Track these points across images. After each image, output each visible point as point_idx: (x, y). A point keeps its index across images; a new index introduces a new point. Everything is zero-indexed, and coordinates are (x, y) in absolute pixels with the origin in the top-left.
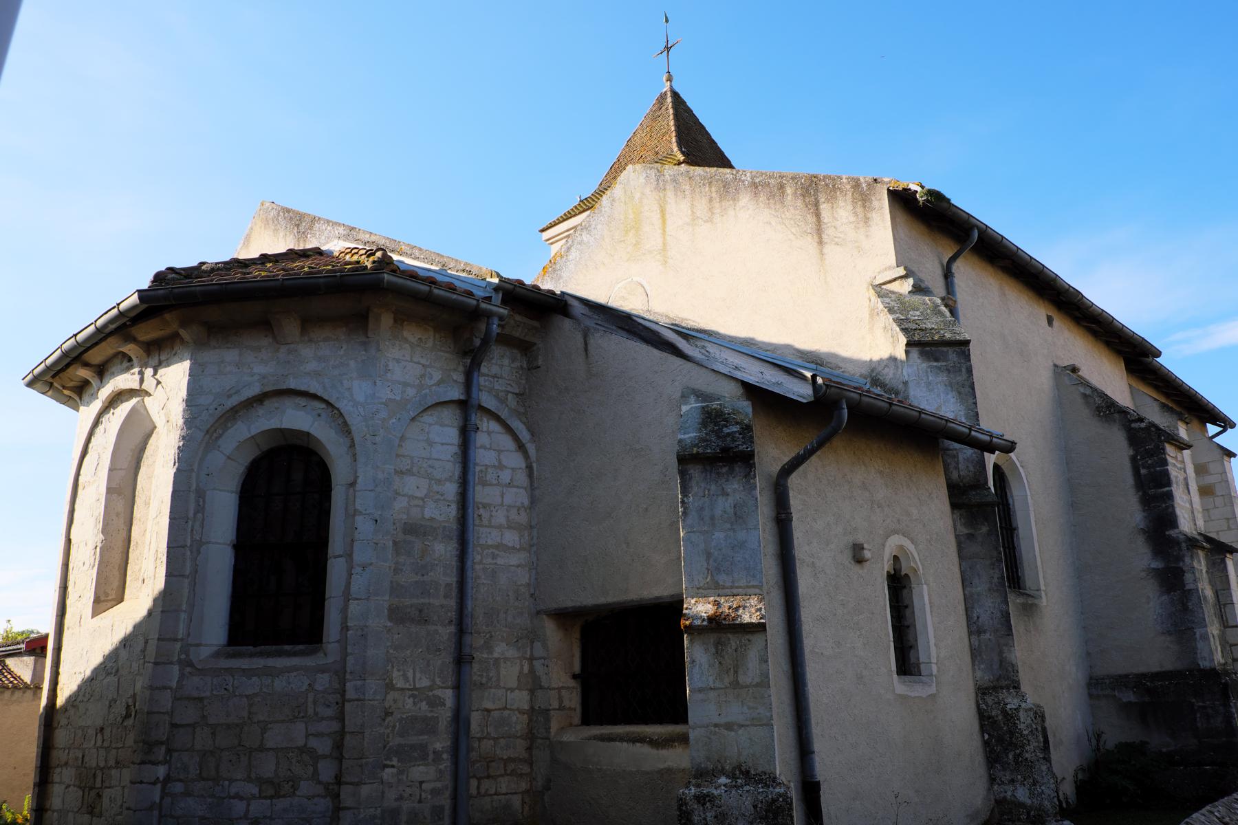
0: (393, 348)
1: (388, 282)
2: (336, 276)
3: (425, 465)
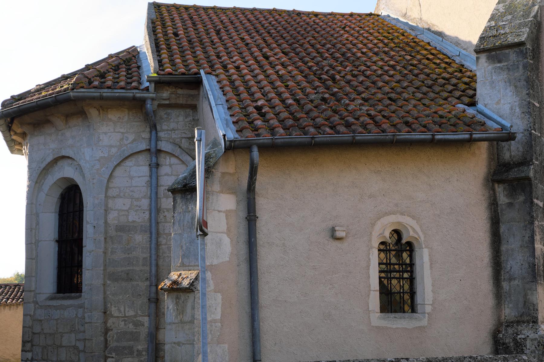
0: (102, 127)
1: (74, 97)
2: (53, 97)
3: (128, 191)
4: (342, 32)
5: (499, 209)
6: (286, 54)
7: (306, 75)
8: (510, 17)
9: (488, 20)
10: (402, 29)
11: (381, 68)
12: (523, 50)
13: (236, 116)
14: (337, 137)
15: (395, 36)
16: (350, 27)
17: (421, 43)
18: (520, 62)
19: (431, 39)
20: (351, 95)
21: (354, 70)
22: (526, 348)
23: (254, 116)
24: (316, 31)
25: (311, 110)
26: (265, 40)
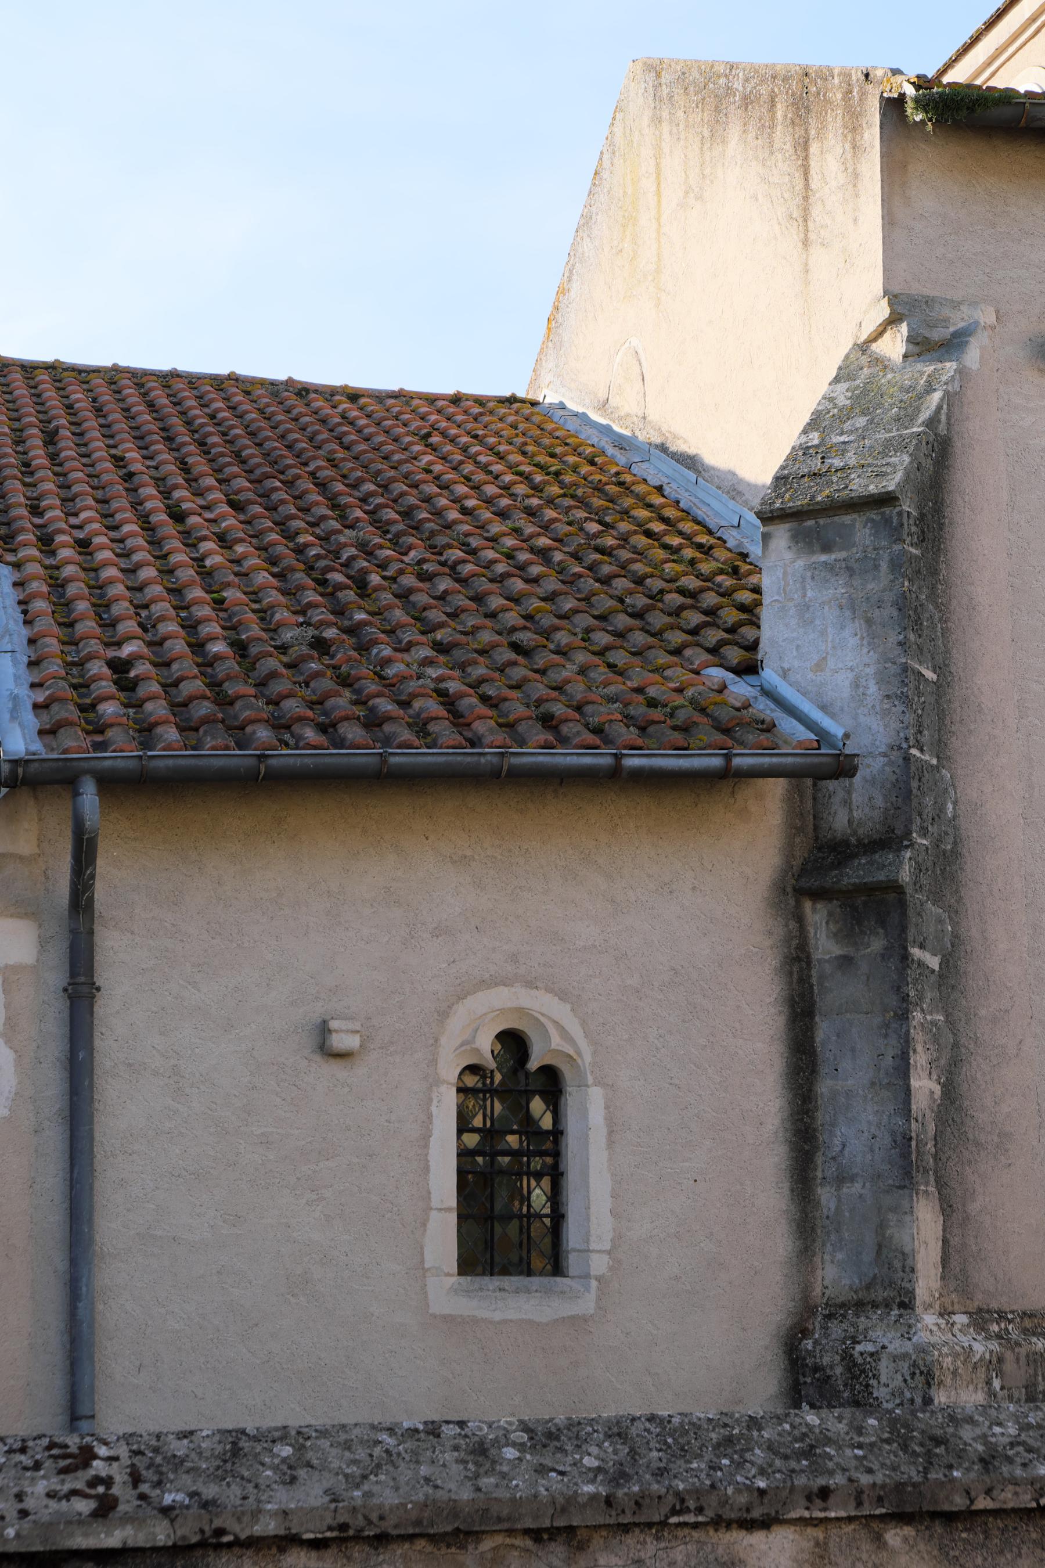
4: (417, 448)
5: (814, 973)
6: (237, 506)
7: (283, 569)
8: (861, 421)
9: (802, 428)
10: (593, 446)
11: (509, 556)
12: (891, 517)
13: (47, 689)
14: (334, 757)
15: (568, 466)
16: (443, 434)
17: (640, 488)
18: (881, 552)
19: (668, 477)
20: (404, 633)
21: (428, 561)
22: (879, 1382)
23: (99, 689)
24: (341, 443)
25: (273, 675)
26: (186, 463)
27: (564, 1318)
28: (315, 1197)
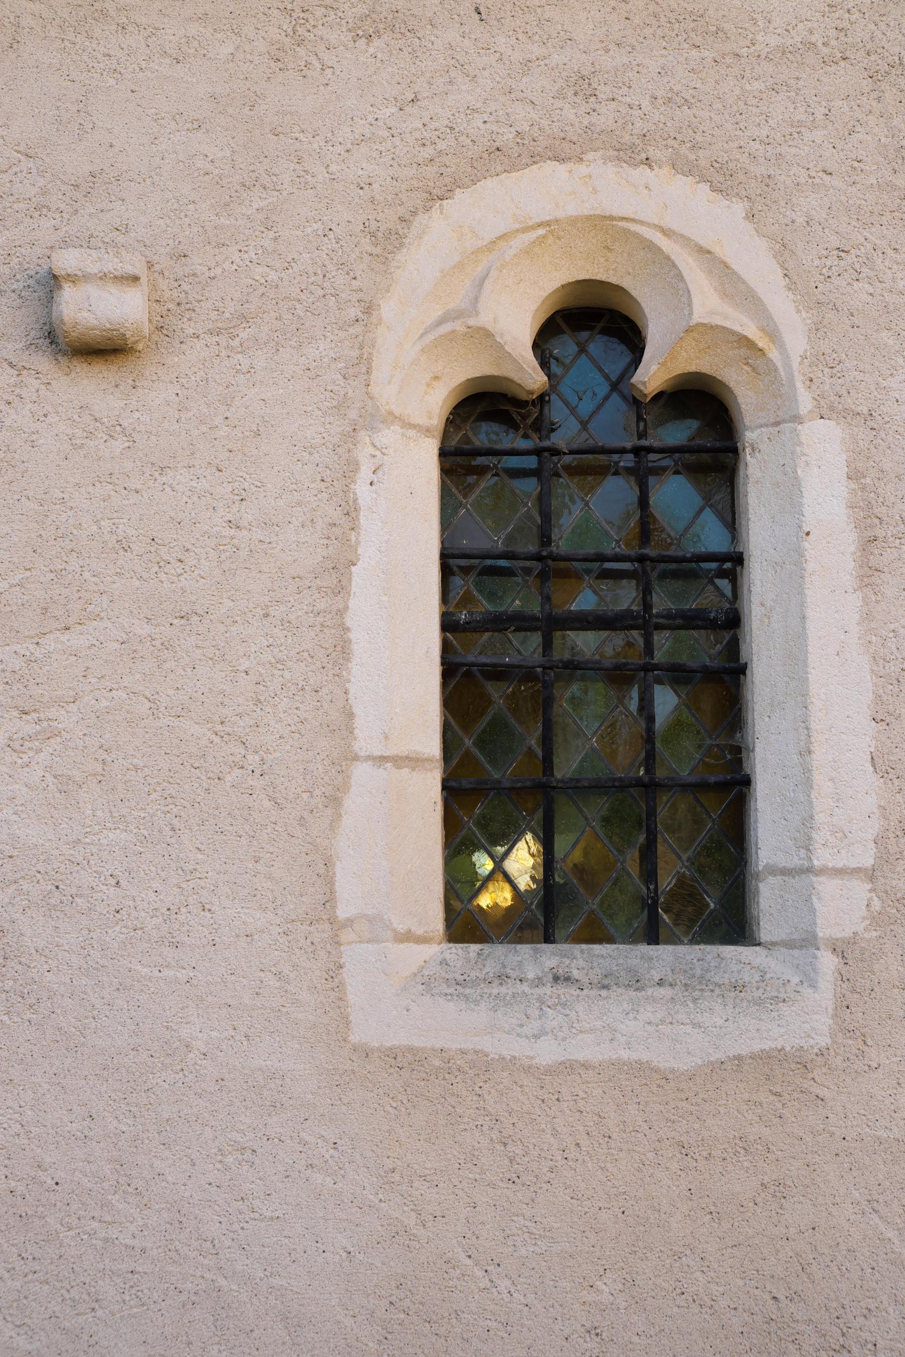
27: (739, 1058)
28: (31, 729)
